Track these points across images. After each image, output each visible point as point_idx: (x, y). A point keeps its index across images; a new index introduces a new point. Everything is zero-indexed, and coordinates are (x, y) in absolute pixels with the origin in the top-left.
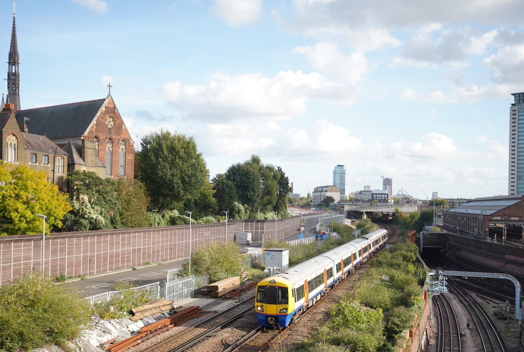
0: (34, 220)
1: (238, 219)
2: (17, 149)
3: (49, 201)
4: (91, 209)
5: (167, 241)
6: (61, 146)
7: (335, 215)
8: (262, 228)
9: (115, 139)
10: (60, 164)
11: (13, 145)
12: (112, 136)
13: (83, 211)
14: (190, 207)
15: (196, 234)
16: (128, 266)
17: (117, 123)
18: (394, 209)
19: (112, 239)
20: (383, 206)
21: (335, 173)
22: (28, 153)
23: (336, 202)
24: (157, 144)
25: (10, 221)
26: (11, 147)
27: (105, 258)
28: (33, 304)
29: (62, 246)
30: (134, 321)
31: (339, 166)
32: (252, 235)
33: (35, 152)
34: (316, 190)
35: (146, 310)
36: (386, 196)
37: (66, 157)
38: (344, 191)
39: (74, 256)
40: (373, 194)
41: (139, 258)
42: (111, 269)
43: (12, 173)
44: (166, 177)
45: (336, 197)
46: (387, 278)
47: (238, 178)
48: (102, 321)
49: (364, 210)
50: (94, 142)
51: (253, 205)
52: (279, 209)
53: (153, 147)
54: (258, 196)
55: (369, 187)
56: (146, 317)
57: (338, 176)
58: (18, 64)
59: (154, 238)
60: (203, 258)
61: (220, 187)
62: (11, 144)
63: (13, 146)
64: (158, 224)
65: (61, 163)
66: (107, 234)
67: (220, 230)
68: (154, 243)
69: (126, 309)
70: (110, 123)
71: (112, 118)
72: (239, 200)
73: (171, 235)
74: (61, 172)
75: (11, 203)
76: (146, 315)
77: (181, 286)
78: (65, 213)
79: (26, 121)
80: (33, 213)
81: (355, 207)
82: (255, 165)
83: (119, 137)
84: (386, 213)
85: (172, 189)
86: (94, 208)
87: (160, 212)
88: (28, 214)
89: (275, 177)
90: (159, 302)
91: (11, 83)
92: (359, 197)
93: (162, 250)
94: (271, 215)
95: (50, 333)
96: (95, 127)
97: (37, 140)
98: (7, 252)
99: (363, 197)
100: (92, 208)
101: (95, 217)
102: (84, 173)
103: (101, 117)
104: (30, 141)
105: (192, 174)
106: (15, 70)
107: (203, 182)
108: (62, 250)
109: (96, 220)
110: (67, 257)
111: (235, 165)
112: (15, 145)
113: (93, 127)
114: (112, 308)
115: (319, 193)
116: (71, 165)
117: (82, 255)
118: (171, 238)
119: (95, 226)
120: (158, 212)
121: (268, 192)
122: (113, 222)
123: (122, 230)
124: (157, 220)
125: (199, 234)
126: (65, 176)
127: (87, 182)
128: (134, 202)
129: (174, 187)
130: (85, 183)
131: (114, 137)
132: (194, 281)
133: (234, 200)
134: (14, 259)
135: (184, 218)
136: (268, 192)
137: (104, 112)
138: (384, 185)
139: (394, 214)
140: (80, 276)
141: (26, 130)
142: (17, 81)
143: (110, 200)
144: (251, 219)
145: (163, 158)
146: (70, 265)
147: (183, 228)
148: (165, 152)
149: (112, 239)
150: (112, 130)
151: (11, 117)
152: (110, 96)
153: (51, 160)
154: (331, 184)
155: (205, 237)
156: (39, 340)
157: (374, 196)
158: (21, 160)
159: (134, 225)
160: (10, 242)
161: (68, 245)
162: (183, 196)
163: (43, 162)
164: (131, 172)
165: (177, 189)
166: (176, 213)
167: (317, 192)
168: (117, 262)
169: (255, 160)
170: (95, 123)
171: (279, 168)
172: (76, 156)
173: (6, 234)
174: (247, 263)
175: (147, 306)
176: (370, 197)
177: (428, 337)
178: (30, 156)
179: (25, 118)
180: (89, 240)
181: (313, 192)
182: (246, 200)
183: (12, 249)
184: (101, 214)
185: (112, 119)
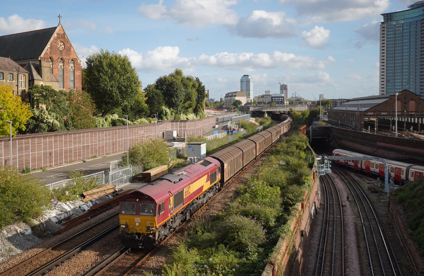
1: (166, 120)
3: (14, 110)
5: (109, 139)
6: (23, 66)
8: (185, 127)
10: (22, 80)
12: (63, 57)
13: (42, 117)
15: (133, 132)
16: (79, 160)
19: (66, 138)
20: (280, 106)
21: (242, 81)
23: (243, 104)
24: (99, 61)
27: (61, 154)
32: (177, 132)
34: (227, 96)
36: (283, 98)
37: (27, 75)
40: (272, 97)
41: (88, 153)
42: (66, 162)
44: (107, 88)
45: (243, 100)
46: (284, 163)
47: (164, 87)
49: (265, 110)
50: (49, 62)
51: (177, 109)
52: (197, 111)
54: (181, 102)
55: (269, 92)
57: (244, 84)
59: (99, 137)
64: (102, 125)
65: (23, 80)
66: (62, 135)
67: (151, 129)
68: (99, 141)
70: (61, 46)
72: (166, 104)
73: (113, 134)
74: (24, 86)
77: (121, 174)
78: (28, 119)
82: (179, 77)
85: (112, 98)
86: (51, 114)
90: (104, 187)
92: (261, 100)
93: (106, 146)
94: (191, 116)
95: (19, 213)
96: (49, 50)
99: (264, 100)
101: (51, 121)
108: (27, 148)
109: (52, 124)
111: (162, 77)
113: (47, 49)
114: (67, 193)
115: (230, 98)
116: (31, 81)
118: (113, 136)
119: (52, 129)
120: (102, 116)
121: (188, 98)
126: (27, 90)
127: (44, 93)
130: (43, 94)
131: (64, 57)
132: (131, 169)
133: (162, 105)
138: (281, 90)
140: (41, 168)
146: (34, 160)
149: (66, 138)
152: (61, 24)
153: (15, 77)
155: (140, 135)
157: (273, 99)
162: (121, 103)
163: (9, 79)
164: (79, 85)
166: (116, 117)
167: (227, 97)
168: (70, 156)
169: (178, 73)
170: (49, 46)
171: (197, 78)
172: (35, 73)
175: (95, 190)
176: (270, 100)
181: (225, 97)
182: (171, 105)
184: (57, 119)
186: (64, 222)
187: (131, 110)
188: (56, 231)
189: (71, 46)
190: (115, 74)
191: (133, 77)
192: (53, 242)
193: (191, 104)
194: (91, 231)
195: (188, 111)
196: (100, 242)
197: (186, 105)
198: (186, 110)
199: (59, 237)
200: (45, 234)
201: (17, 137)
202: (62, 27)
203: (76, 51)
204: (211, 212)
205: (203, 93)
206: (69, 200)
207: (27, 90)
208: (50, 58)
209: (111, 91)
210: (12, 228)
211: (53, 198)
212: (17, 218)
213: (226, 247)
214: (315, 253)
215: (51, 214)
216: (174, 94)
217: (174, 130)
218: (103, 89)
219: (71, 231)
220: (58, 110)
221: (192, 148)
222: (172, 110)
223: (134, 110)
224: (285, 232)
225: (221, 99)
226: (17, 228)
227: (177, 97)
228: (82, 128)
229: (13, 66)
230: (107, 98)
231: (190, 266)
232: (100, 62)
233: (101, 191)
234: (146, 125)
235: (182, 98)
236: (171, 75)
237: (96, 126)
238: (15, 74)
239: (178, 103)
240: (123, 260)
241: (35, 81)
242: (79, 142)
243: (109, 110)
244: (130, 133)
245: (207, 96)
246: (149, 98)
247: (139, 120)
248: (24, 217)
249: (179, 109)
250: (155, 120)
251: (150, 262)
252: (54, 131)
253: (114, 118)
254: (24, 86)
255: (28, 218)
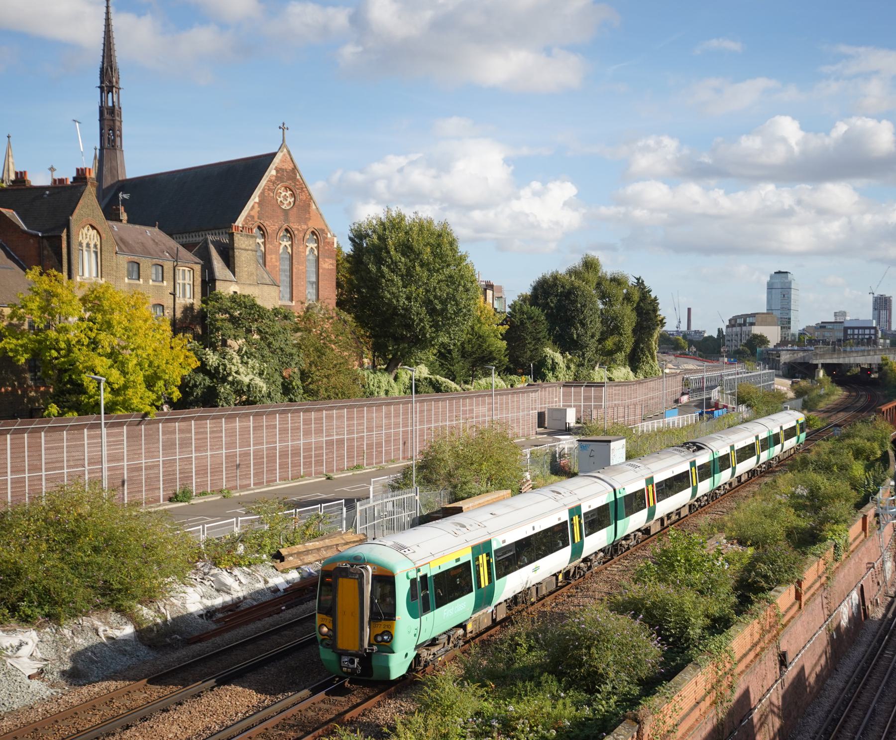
0: (125, 387)
1: (553, 380)
2: (99, 253)
3: (155, 350)
4: (240, 365)
5: (397, 425)
6: (188, 247)
7: (761, 371)
8: (599, 398)
9: (298, 230)
10: (187, 281)
11: (92, 246)
12: (291, 225)
13: (225, 370)
14: (452, 359)
15: (458, 410)
16: (319, 474)
17: (301, 200)
18: (880, 357)
19: (284, 421)
20: (857, 352)
21: (770, 287)
22: (123, 261)
23: (771, 346)
24: (379, 238)
25: (80, 389)
26: (89, 251)
27: (271, 459)
28: (73, 537)
29: (183, 436)
30: (282, 572)
31: (780, 272)
32: (578, 412)
33: (136, 259)
34: (733, 322)
35: (308, 552)
36: (873, 331)
37: (198, 268)
38: (789, 322)
39: (209, 453)
40: (846, 329)
41: (341, 457)
42: (284, 479)
43: (84, 300)
44: (398, 301)
45: (772, 334)
46: (805, 493)
47: (553, 302)
48: (215, 571)
49: (819, 361)
50: (253, 237)
51: (583, 354)
52: (639, 360)
53: (373, 245)
54: (593, 336)
55: (844, 314)
56: (307, 564)
57: (777, 293)
58: (119, 89)
59: (370, 420)
60: (439, 456)
61: (517, 321)
62: (88, 245)
63: (92, 249)
64: (387, 392)
65: (188, 280)
66: (274, 413)
67: (507, 403)
68: (370, 429)
69: (267, 549)
70: (285, 199)
71: (291, 190)
72: (555, 342)
73: (405, 413)
74: (188, 295)
75: (81, 356)
76: (306, 561)
77: (390, 507)
78: (185, 372)
79: (124, 200)
80: (124, 373)
81: (801, 354)
82: (590, 276)
83: (305, 227)
84: (866, 366)
85: (409, 327)
86: (247, 363)
87: (390, 369)
88: (115, 374)
89: (628, 298)
90: (338, 538)
91: (106, 128)
92: (817, 335)
93: (388, 442)
94: (622, 372)
95: (106, 590)
96: (257, 209)
97: (140, 237)
98: (75, 446)
99: (827, 334)
100: (242, 362)
101: (246, 380)
102: (234, 298)
103: (271, 188)
104: (126, 237)
105: (448, 294)
106: (113, 102)
107: (469, 311)
108: (185, 444)
109: (248, 386)
110: (194, 455)
111: (548, 276)
112: (95, 246)
113: (253, 207)
114: (241, 549)
115: (738, 329)
116: (208, 283)
117: (224, 451)
118: (405, 419)
119: (247, 398)
120: (386, 370)
121: (612, 327)
122: (287, 389)
123: (305, 405)
124: (384, 385)
125: (465, 412)
126: (197, 304)
127: (237, 313)
128: (333, 350)
129: (413, 321)
130: (231, 316)
131: (294, 226)
132: (417, 498)
133: (543, 345)
134: (89, 460)
135: (437, 381)
136: (612, 327)
137: (274, 178)
138: (875, 309)
139: (880, 368)
140: (221, 491)
141: (124, 216)
142: (117, 124)
143: (281, 349)
144: (576, 382)
145: (388, 267)
146: (201, 471)
147: (431, 400)
148: (392, 253)
149: (284, 421)
150: (291, 212)
151: (86, 193)
152: (286, 147)
153: (169, 274)
154: (764, 310)
155: (477, 417)
156: (84, 603)
157: (849, 332)
158: (108, 274)
159: (332, 395)
160: (81, 427)
161: (196, 433)
162: (433, 338)
163: (154, 277)
164: (330, 295)
165: (418, 324)
166: (422, 371)
167: (733, 326)
168: (296, 465)
169: (590, 265)
170: (257, 200)
171: (638, 279)
172: (218, 264)
173: (76, 414)
174: (543, 465)
175: (310, 545)
176: (841, 335)
177: (868, 603)
178: (126, 266)
179: (120, 195)
180: (237, 424)
181: (728, 327)
182: (567, 344)
183: (86, 442)
184: (261, 374)
185: (290, 192)
186: (221, 615)
187: (463, 356)
188: (196, 634)
189: (311, 198)
190: (418, 268)
191: (462, 277)
192: (178, 658)
193: (620, 341)
194: (275, 637)
195: (615, 361)
196: (282, 661)
197: (609, 343)
198: (608, 357)
199: (197, 647)
200: (168, 640)
201: (157, 415)
202: (289, 152)
203: (322, 211)
204: (576, 602)
205: (652, 315)
206: (240, 565)
207: (197, 304)
208: (259, 228)
209: (407, 310)
210: (85, 624)
211: (203, 559)
212: (98, 600)
213: (560, 681)
214: (826, 709)
215: (193, 599)
216: (577, 321)
217: (570, 406)
218: (390, 304)
219: (227, 636)
220: (266, 352)
221: (590, 450)
222: (570, 357)
223: (471, 355)
224: (710, 652)
225: (720, 331)
226: (97, 623)
227: (583, 325)
228: (329, 398)
229: (163, 247)
230: (398, 326)
231: (456, 725)
232: (382, 238)
233: (328, 548)
234: (500, 392)
235: (597, 326)
236: (573, 272)
237: (372, 394)
238: (168, 265)
239: (586, 339)
240: (322, 705)
241: (217, 283)
242: (319, 431)
243: (403, 356)
244: (451, 411)
245: (662, 323)
246: (512, 326)
247: (483, 381)
248: (118, 599)
249: (588, 355)
250: (522, 382)
251: (381, 709)
252: (253, 403)
253: (416, 375)
254: (188, 295)
255: (126, 603)
